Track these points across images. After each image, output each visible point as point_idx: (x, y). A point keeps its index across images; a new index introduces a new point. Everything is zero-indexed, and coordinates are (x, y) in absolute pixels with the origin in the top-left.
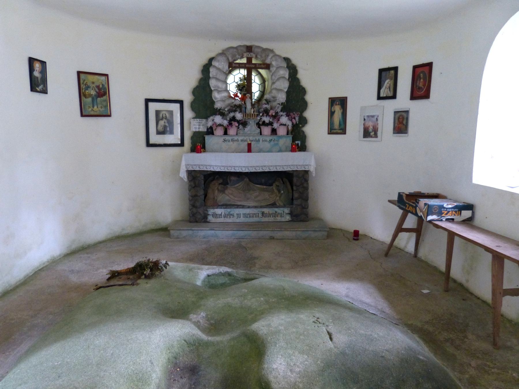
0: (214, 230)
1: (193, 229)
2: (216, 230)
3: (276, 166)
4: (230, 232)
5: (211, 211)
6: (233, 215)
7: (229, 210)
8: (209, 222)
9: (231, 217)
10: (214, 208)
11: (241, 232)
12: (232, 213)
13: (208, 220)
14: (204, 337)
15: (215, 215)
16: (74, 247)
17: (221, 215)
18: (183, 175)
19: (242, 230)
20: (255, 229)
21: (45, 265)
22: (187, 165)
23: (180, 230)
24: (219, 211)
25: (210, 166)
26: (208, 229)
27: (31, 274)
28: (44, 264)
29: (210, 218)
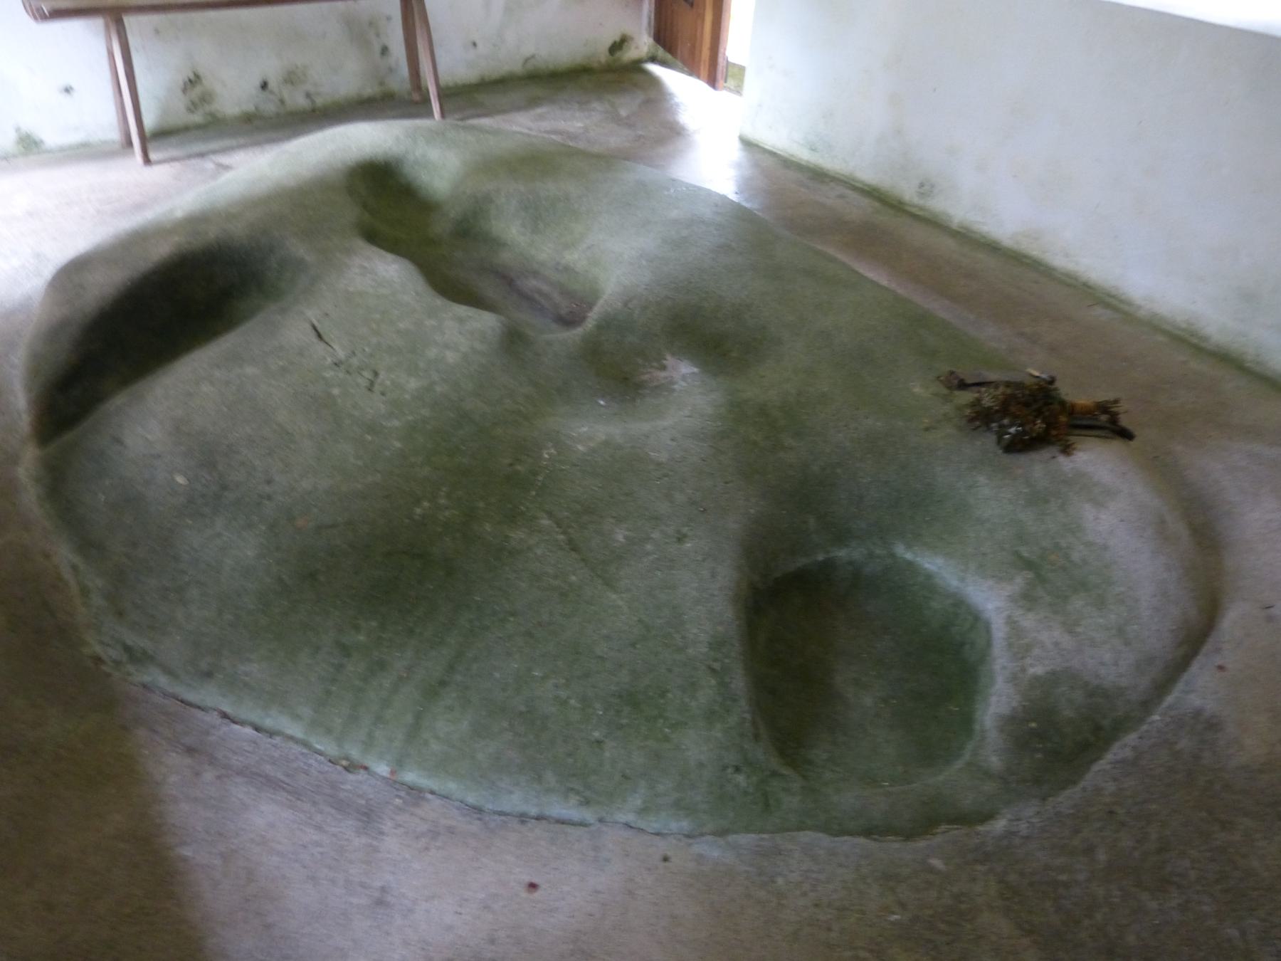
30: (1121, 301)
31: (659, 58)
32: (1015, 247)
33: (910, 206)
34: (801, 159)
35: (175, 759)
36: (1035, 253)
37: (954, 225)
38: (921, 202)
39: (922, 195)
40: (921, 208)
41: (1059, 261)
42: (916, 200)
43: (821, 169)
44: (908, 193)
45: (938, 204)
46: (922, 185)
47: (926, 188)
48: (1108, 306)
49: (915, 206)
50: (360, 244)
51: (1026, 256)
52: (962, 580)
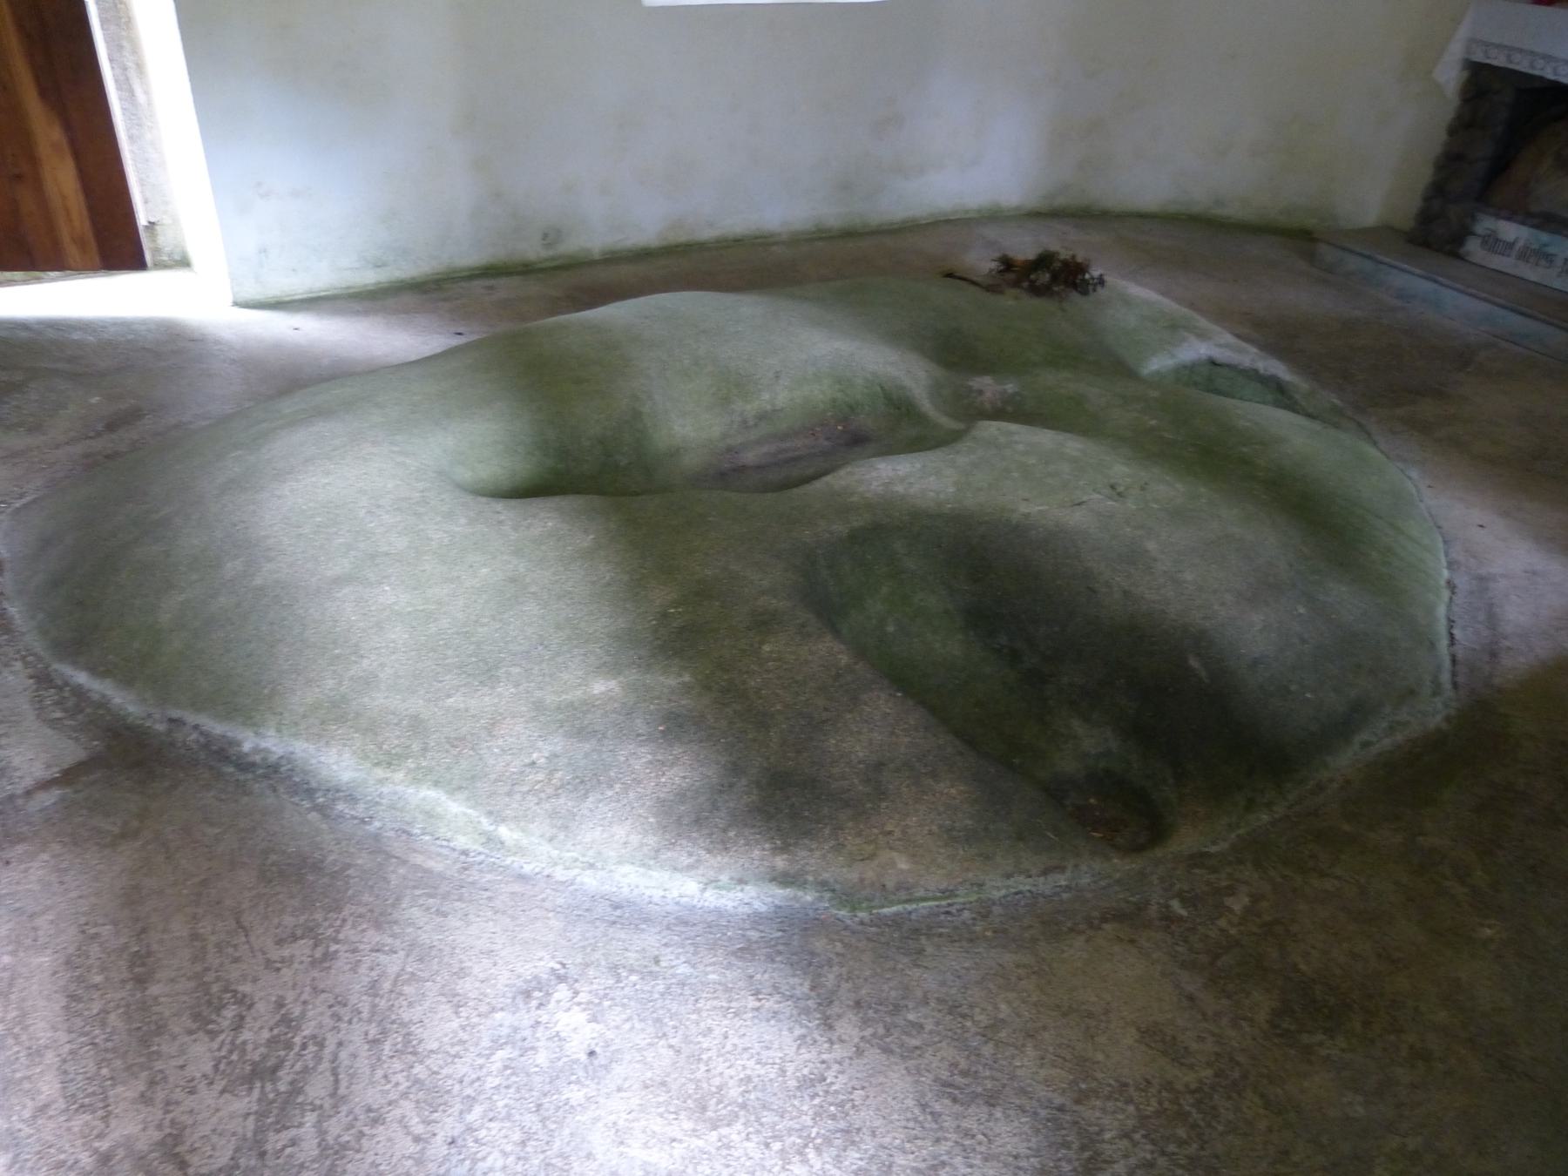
0: (1436, 281)
1: (1380, 258)
2: (1442, 284)
3: (1511, 49)
4: (1483, 307)
5: (1486, 224)
6: (1549, 258)
7: (1545, 237)
8: (1467, 261)
9: (1543, 262)
10: (1498, 216)
11: (1519, 319)
12: (1550, 250)
13: (1462, 251)
14: (926, 406)
15: (1493, 243)
16: (1061, 201)
17: (1511, 245)
18: (1450, 76)
19: (1470, 295)
20: (1474, 291)
21: (968, 216)
22: (1472, 42)
23: (1344, 249)
24: (1510, 231)
25: (1548, 58)
26: (1418, 271)
27: (924, 222)
28: (967, 212)
29: (1473, 247)
30: (766, 237)
31: (410, 1138)
32: (664, 243)
33: (541, 262)
34: (366, 285)
35: (1507, 661)
36: (682, 238)
37: (597, 257)
38: (551, 253)
39: (549, 246)
40: (553, 259)
41: (706, 234)
42: (544, 254)
43: (402, 281)
44: (532, 250)
45: (573, 244)
46: (545, 236)
47: (551, 236)
48: (80, 329)
49: (546, 260)
50: (506, 844)
51: (677, 246)
52: (1173, 356)
